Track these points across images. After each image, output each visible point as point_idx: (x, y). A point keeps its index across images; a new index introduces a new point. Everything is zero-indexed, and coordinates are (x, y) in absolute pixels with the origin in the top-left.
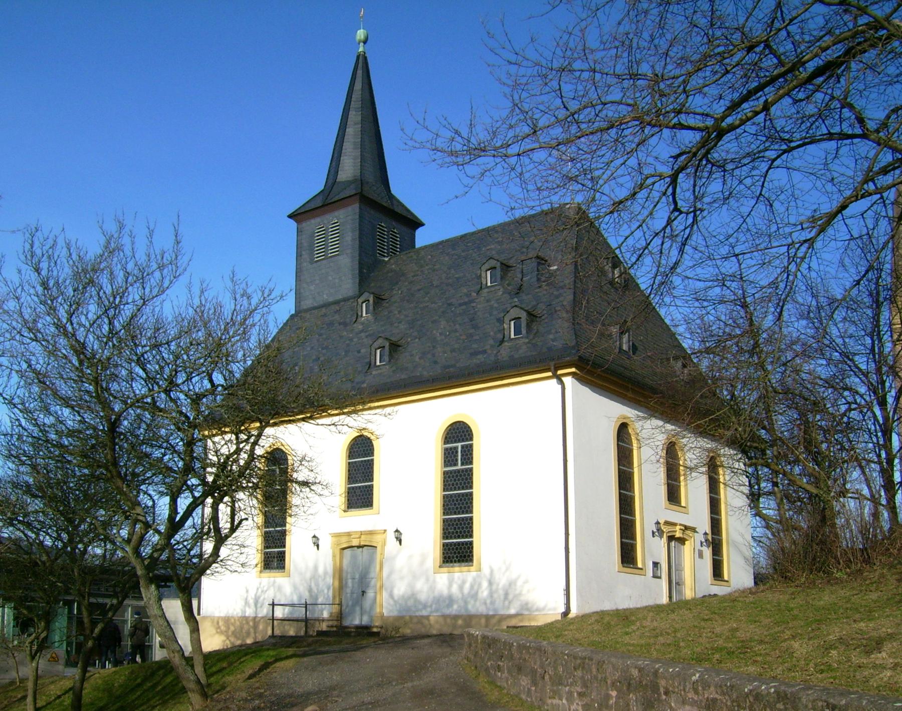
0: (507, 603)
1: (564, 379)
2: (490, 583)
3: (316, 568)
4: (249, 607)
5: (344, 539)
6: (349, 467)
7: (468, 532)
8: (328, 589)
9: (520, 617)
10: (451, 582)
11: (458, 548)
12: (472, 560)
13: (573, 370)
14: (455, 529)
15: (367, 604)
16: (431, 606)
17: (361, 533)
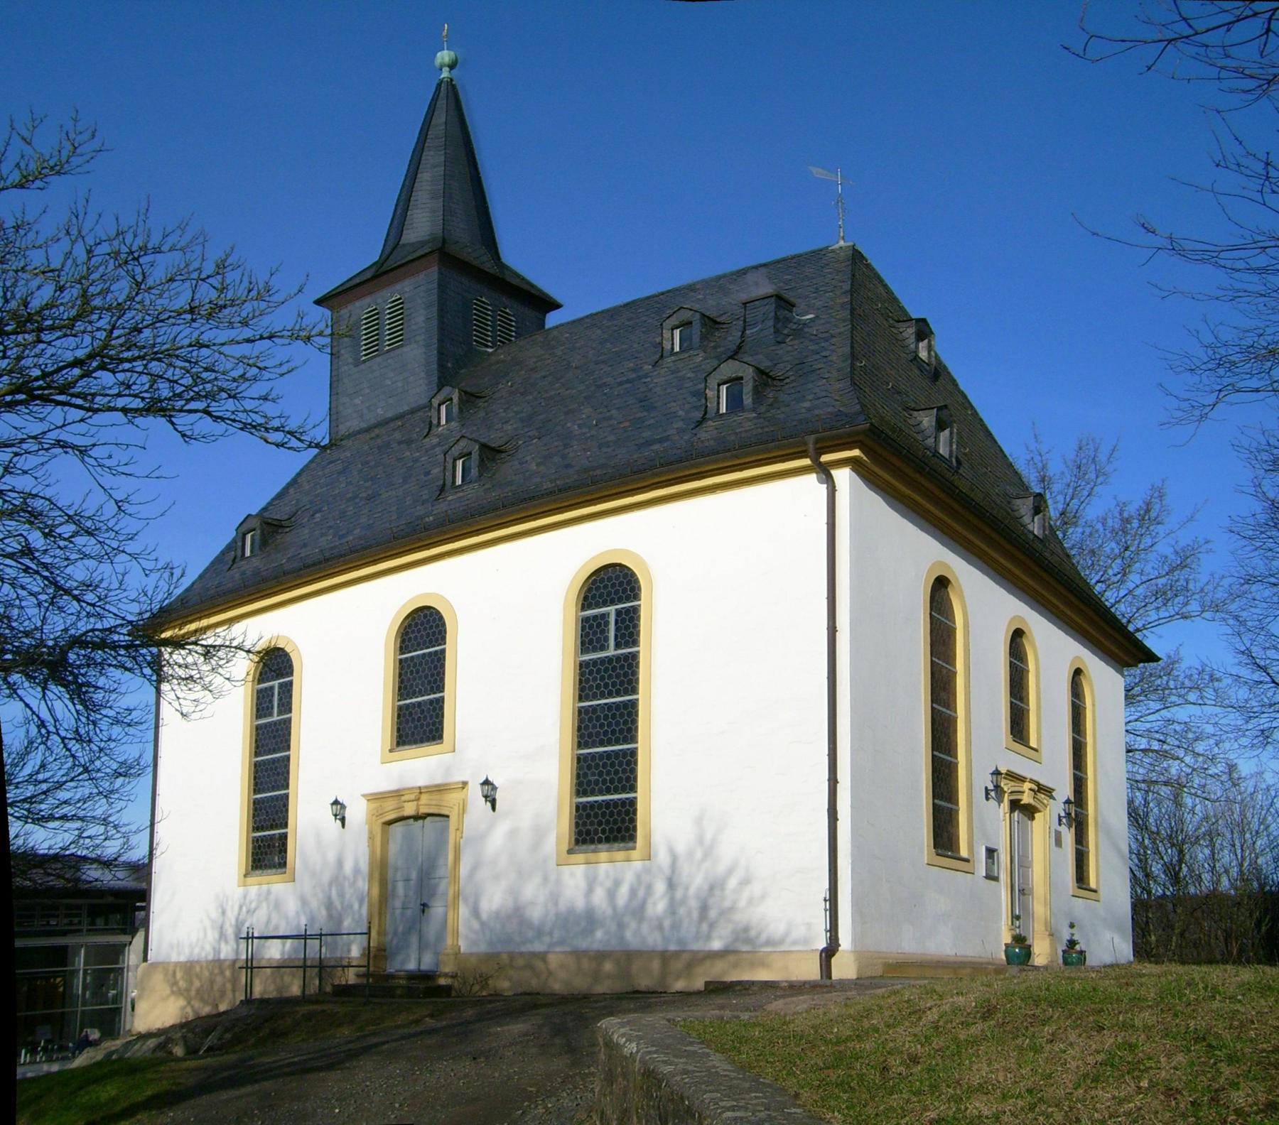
0: (705, 927)
1: (834, 472)
2: (671, 885)
3: (340, 863)
4: (226, 942)
5: (390, 804)
6: (401, 668)
7: (628, 779)
8: (361, 902)
9: (731, 958)
10: (589, 884)
11: (605, 807)
12: (632, 838)
13: (856, 452)
14: (602, 678)
15: (431, 930)
16: (551, 934)
17: (420, 791)
